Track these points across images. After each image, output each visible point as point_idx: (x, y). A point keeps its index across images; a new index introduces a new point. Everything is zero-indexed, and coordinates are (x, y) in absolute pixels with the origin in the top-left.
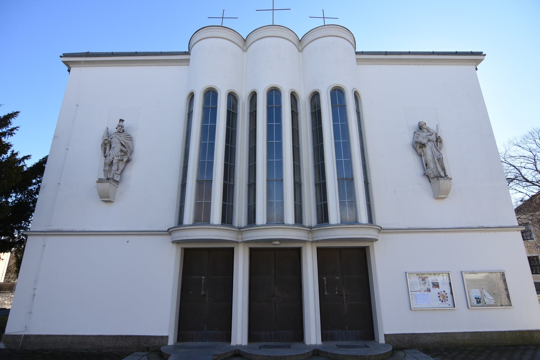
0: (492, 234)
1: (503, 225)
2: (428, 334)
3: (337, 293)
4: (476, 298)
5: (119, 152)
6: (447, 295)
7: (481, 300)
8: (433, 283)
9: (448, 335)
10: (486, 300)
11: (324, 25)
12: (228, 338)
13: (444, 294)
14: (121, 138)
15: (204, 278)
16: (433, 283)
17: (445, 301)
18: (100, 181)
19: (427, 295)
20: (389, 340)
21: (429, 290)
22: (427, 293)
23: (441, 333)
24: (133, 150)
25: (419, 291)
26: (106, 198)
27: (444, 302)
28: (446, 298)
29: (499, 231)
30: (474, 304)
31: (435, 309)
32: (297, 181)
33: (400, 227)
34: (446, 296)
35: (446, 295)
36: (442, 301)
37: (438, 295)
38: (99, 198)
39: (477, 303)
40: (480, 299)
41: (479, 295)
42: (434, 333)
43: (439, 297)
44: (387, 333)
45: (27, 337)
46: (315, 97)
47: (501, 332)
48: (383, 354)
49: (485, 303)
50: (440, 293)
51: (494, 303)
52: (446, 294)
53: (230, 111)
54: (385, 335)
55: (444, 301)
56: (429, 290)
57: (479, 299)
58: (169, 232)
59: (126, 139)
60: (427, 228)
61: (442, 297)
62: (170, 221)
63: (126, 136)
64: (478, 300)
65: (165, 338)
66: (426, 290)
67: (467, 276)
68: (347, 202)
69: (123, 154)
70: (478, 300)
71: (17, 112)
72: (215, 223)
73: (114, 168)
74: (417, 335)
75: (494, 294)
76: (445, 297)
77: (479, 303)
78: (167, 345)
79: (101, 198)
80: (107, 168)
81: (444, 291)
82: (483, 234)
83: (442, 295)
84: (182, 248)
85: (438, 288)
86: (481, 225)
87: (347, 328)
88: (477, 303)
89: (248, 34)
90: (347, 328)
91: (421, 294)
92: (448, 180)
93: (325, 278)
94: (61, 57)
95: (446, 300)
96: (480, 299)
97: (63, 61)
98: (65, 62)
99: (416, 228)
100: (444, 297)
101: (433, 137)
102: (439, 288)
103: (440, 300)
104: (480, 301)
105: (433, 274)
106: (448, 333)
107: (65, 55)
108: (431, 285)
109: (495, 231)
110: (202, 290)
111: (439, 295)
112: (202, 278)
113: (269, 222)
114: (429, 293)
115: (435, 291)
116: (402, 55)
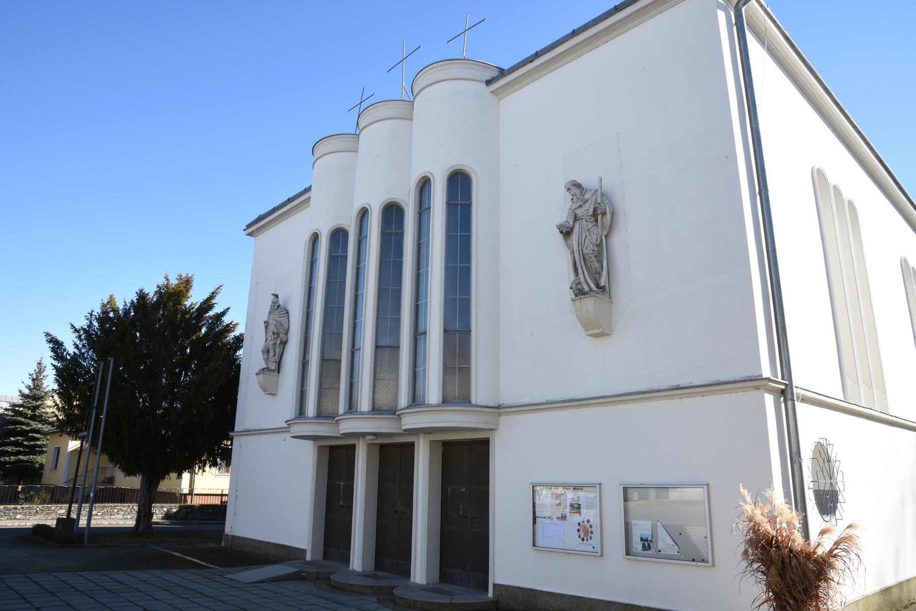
0: (697, 400)
2: (551, 593)
4: (642, 539)
6: (592, 529)
7: (651, 544)
8: (572, 506)
9: (583, 602)
10: (661, 546)
11: (354, 133)
13: (588, 525)
19: (561, 525)
20: (497, 593)
21: (563, 518)
22: (560, 522)
23: (571, 596)
27: (585, 542)
28: (590, 535)
29: (710, 393)
30: (637, 551)
31: (571, 552)
32: (330, 355)
33: (533, 401)
34: (590, 530)
35: (591, 528)
36: (583, 540)
37: (578, 527)
39: (643, 550)
40: (650, 541)
41: (647, 533)
42: (560, 595)
43: (579, 530)
45: (233, 537)
49: (660, 551)
50: (582, 524)
51: (678, 552)
52: (591, 526)
54: (495, 585)
55: (585, 538)
57: (647, 540)
59: (279, 317)
60: (575, 398)
61: (584, 531)
63: (280, 313)
66: (560, 516)
68: (457, 370)
70: (646, 543)
71: (228, 308)
72: (309, 416)
73: (271, 354)
74: (535, 592)
75: (680, 534)
76: (588, 531)
77: (647, 550)
79: (264, 391)
81: (588, 521)
82: (686, 401)
83: (585, 528)
84: (432, 443)
86: (676, 383)
87: (468, 568)
88: (643, 550)
90: (468, 568)
91: (551, 524)
92: (588, 298)
93: (342, 483)
94: (244, 230)
95: (589, 538)
97: (491, 92)
98: (248, 235)
99: (558, 400)
100: (586, 534)
101: (589, 208)
102: (580, 515)
103: (580, 537)
104: (649, 545)
105: (572, 488)
106: (582, 597)
107: (249, 226)
108: (568, 509)
109: (703, 394)
110: (341, 499)
113: (320, 415)
114: (564, 522)
116: (557, 46)
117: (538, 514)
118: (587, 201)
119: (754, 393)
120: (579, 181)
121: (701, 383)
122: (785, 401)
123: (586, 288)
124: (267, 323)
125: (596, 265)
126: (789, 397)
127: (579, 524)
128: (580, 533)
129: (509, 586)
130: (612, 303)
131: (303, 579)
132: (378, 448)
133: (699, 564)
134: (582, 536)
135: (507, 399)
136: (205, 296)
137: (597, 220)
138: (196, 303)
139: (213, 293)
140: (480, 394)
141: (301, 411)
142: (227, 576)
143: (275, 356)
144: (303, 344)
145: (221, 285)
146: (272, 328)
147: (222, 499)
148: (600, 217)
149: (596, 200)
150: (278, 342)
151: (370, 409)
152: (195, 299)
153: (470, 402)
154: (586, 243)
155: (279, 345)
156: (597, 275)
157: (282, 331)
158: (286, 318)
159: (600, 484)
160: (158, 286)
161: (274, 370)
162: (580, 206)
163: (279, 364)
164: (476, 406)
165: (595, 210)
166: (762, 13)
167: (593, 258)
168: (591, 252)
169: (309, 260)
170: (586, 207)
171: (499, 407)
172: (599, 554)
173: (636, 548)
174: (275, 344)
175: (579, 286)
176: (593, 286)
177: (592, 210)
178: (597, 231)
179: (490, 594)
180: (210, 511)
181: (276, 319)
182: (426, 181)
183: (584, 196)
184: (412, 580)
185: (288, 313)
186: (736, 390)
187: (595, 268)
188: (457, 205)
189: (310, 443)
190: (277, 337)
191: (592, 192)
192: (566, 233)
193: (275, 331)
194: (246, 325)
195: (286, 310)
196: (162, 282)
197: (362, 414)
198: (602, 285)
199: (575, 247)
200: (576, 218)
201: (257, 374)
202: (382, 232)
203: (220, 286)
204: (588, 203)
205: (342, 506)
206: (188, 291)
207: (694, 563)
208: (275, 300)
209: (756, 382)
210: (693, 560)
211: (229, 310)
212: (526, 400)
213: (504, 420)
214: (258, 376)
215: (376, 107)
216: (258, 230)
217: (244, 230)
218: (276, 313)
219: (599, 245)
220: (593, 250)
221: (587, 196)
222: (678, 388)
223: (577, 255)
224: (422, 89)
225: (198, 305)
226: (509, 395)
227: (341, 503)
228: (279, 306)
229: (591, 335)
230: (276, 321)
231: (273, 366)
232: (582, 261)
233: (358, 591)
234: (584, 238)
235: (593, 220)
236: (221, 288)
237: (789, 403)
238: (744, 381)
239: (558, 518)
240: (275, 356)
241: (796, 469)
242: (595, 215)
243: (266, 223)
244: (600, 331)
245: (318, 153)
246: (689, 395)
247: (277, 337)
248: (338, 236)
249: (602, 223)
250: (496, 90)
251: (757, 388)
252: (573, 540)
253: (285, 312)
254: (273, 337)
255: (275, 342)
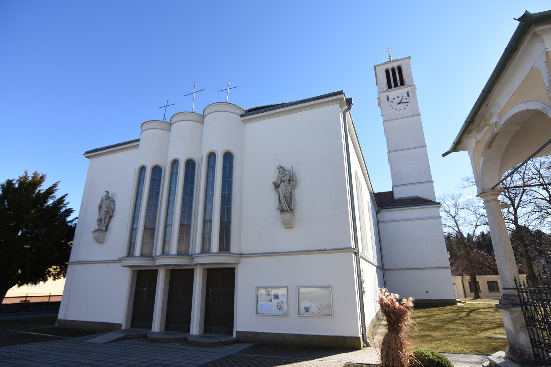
1: (338, 247)
3: (217, 300)
4: (305, 308)
5: (105, 213)
11: (162, 120)
12: (150, 327)
14: (106, 203)
15: (146, 289)
16: (275, 295)
17: (281, 309)
18: (95, 231)
21: (271, 301)
22: (269, 303)
24: (114, 209)
25: (264, 301)
26: (100, 241)
29: (333, 253)
31: (304, 316)
36: (279, 309)
38: (95, 241)
40: (309, 309)
44: (239, 330)
45: (65, 321)
46: (191, 164)
47: (320, 336)
48: (214, 342)
49: (312, 312)
50: (279, 303)
52: (283, 304)
53: (189, 174)
54: (237, 332)
55: (280, 309)
56: (271, 301)
57: (307, 308)
58: (120, 260)
62: (123, 252)
64: (307, 310)
65: (120, 325)
67: (302, 290)
69: (107, 213)
70: (307, 310)
71: (67, 194)
73: (103, 222)
77: (307, 312)
78: (121, 329)
80: (99, 223)
81: (282, 302)
84: (204, 269)
85: (277, 299)
86: (319, 248)
89: (234, 104)
94: (84, 154)
96: (309, 309)
97: (242, 120)
101: (287, 178)
102: (278, 299)
103: (278, 308)
107: (87, 153)
108: (273, 297)
111: (278, 305)
112: (145, 289)
114: (271, 302)
115: (275, 301)
117: (258, 300)
118: (286, 175)
119: (349, 253)
120: (282, 166)
121: (329, 249)
122: (356, 256)
123: (286, 210)
124: (100, 207)
125: (290, 201)
126: (357, 255)
127: (278, 303)
128: (278, 307)
129: (244, 332)
130: (294, 216)
131: (129, 339)
132: (170, 271)
133: (328, 316)
134: (279, 308)
135: (244, 251)
136: (51, 185)
137: (290, 183)
138: (43, 189)
139: (54, 185)
140: (234, 248)
141: (130, 253)
142: (86, 341)
143: (105, 223)
144: (132, 220)
145: (59, 181)
146: (104, 209)
147: (26, 299)
148: (291, 182)
149: (290, 175)
150: (108, 216)
151: (177, 253)
152: (44, 187)
153: (230, 252)
154: (286, 192)
155: (109, 218)
156: (290, 205)
157: (110, 210)
158: (113, 204)
159: (287, 287)
160: (20, 177)
161: (104, 231)
162: (284, 176)
163: (107, 227)
164: (233, 254)
165: (290, 179)
166: (351, 121)
167: (289, 198)
168: (288, 195)
169: (138, 179)
170: (286, 177)
171: (241, 254)
172: (287, 315)
173: (302, 312)
174: (106, 217)
175: (282, 208)
176: (288, 209)
177: (288, 179)
178: (290, 187)
179: (234, 336)
180: (17, 307)
181: (108, 204)
182: (212, 154)
183: (285, 172)
184: (191, 333)
185: (114, 201)
186: (343, 252)
187: (289, 202)
188: (227, 167)
189: (128, 269)
190: (107, 214)
191: (288, 172)
192: (277, 186)
193: (107, 210)
194: (82, 205)
195: (113, 200)
196: (22, 174)
197: (172, 256)
198: (292, 209)
199: (281, 192)
200: (282, 181)
201: (93, 232)
202: (185, 172)
203: (59, 182)
204: (287, 175)
205: (145, 300)
206: (41, 182)
207: (326, 316)
208: (107, 194)
209: (348, 249)
210: (326, 315)
211: (68, 195)
212: (254, 252)
213: (243, 260)
214: (93, 233)
215: (184, 114)
216: (94, 156)
217: (84, 154)
218: (107, 201)
219: (291, 193)
220: (289, 195)
221: (286, 173)
222: (320, 250)
223: (281, 196)
224: (209, 114)
225: (44, 190)
226: (245, 250)
227: (145, 298)
228: (109, 198)
229: (286, 228)
230: (107, 205)
231: (104, 229)
232: (284, 199)
233: (155, 340)
234: (285, 189)
235: (288, 182)
236: (59, 182)
237: (358, 257)
238: (346, 249)
239: (268, 301)
240: (105, 223)
241: (360, 280)
242: (289, 181)
243: (101, 153)
244: (290, 226)
245: (143, 128)
246: (324, 253)
247: (107, 214)
248: (157, 170)
249: (292, 184)
250: (244, 120)
251: (350, 252)
252: (275, 310)
253: (113, 201)
254: (105, 213)
255: (106, 216)
